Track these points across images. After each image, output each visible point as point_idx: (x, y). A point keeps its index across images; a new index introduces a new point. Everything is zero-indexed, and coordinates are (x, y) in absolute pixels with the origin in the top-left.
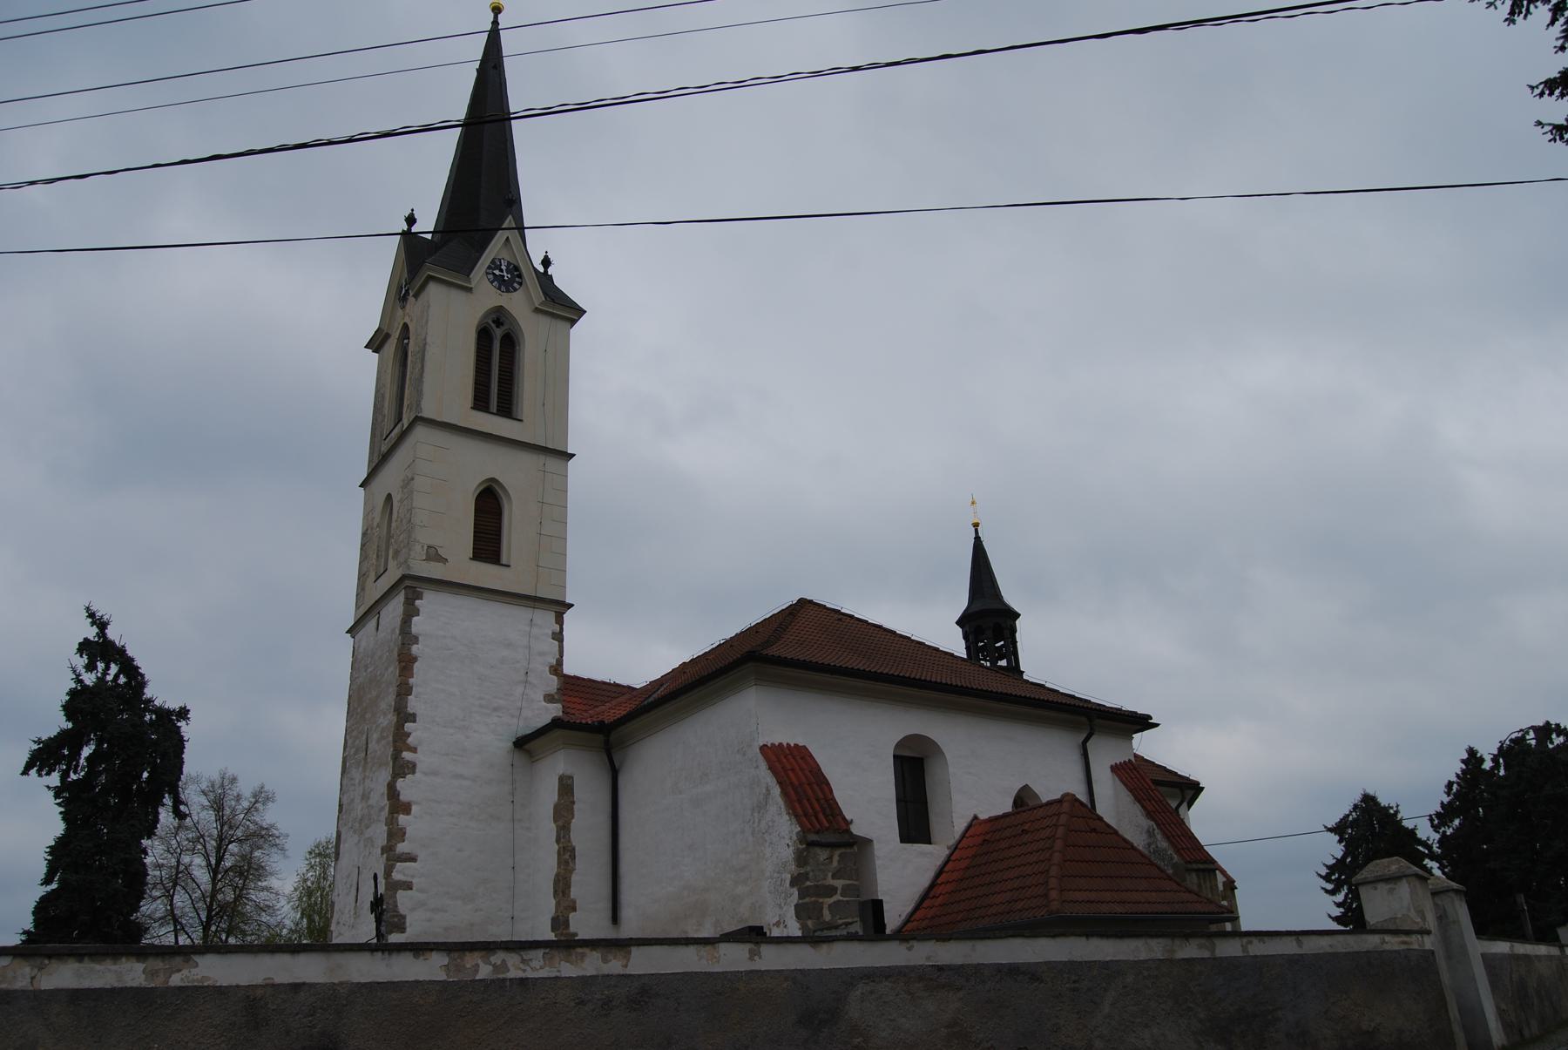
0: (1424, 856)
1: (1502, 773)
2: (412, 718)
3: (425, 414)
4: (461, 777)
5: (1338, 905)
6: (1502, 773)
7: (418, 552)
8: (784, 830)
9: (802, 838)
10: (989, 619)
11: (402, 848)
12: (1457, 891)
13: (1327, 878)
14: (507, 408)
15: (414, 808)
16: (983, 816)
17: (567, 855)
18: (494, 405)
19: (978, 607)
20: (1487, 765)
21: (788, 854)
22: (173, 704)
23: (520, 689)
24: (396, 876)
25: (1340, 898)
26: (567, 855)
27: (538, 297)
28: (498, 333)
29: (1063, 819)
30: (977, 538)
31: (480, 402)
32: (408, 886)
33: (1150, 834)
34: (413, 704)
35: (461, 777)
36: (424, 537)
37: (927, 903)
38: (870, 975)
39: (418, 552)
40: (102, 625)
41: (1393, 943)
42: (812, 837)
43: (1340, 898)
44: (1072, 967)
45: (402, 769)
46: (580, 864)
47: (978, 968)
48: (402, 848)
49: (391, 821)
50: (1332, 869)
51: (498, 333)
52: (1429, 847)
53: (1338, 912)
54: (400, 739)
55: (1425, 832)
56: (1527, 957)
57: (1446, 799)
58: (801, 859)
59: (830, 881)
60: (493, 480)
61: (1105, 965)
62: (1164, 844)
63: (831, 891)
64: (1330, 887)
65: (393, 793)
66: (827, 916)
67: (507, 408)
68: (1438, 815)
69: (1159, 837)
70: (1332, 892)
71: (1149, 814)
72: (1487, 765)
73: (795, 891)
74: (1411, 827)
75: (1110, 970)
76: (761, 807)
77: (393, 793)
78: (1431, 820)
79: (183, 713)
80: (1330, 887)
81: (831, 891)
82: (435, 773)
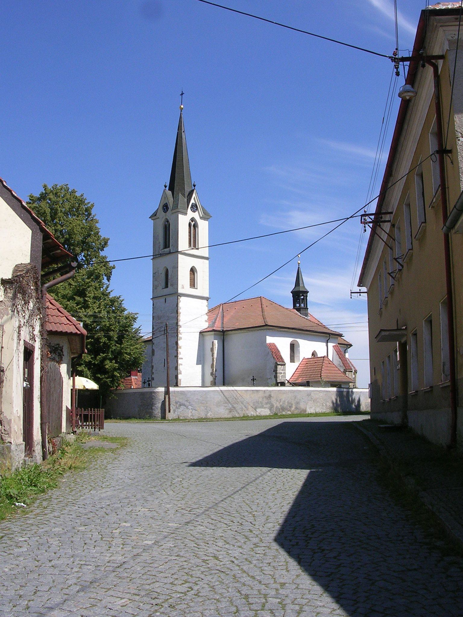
19: (297, 289)
31: (190, 245)
51: (193, 223)
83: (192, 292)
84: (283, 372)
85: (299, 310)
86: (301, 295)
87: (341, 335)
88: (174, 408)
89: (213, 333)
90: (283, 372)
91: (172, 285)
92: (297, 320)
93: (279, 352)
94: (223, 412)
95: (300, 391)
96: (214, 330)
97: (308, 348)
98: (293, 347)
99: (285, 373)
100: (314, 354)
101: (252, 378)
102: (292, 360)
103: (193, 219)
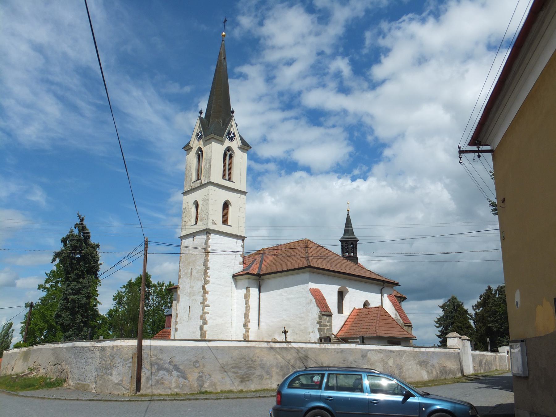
0: (469, 319)
1: (497, 296)
2: (208, 268)
3: (212, 181)
4: (220, 285)
5: (439, 331)
6: (497, 296)
7: (210, 222)
8: (315, 311)
9: (321, 312)
10: (349, 244)
11: (206, 303)
12: (468, 340)
13: (437, 322)
14: (230, 179)
15: (209, 293)
16: (357, 308)
17: (248, 308)
18: (227, 178)
19: (347, 237)
20: (493, 292)
21: (317, 316)
22: (96, 243)
23: (233, 261)
24: (205, 310)
25: (440, 329)
26: (248, 308)
27: (240, 144)
28: (228, 154)
29: (379, 312)
30: (348, 215)
31: (224, 178)
32: (208, 313)
33: (396, 315)
34: (209, 264)
35: (220, 285)
36: (211, 217)
37: (343, 328)
38: (371, 350)
39: (210, 222)
40: (82, 220)
41: (452, 350)
42: (323, 313)
43: (440, 329)
44: (399, 351)
45: (206, 282)
46: (251, 310)
47: (385, 350)
48: (206, 303)
49: (203, 296)
50: (439, 319)
51: (228, 154)
52: (471, 316)
53: (439, 334)
54: (206, 274)
55: (471, 311)
56: (484, 355)
57: (479, 301)
58: (320, 318)
59: (326, 324)
60: (228, 200)
61: (404, 351)
62: (400, 318)
63: (327, 326)
64: (438, 325)
65: (204, 288)
66: (325, 332)
67: (230, 179)
68: (476, 306)
69: (398, 316)
70: (438, 327)
71: (396, 310)
72: (493, 292)
73: (318, 325)
74: (466, 309)
75: (405, 352)
76: (309, 304)
77: (204, 288)
78: (473, 307)
79: (98, 246)
80: (438, 325)
81: (327, 326)
82: (214, 284)
83: (225, 229)
84: (328, 324)
85: (349, 258)
86: (350, 242)
87: (396, 284)
88: (148, 373)
89: (247, 276)
90: (328, 324)
91: (201, 220)
92: (347, 267)
93: (324, 299)
94: (229, 383)
95: (351, 350)
96: (248, 274)
97: (356, 298)
98: (341, 295)
99: (331, 326)
100: (366, 304)
101: (283, 330)
102: (340, 310)
103: (229, 149)
